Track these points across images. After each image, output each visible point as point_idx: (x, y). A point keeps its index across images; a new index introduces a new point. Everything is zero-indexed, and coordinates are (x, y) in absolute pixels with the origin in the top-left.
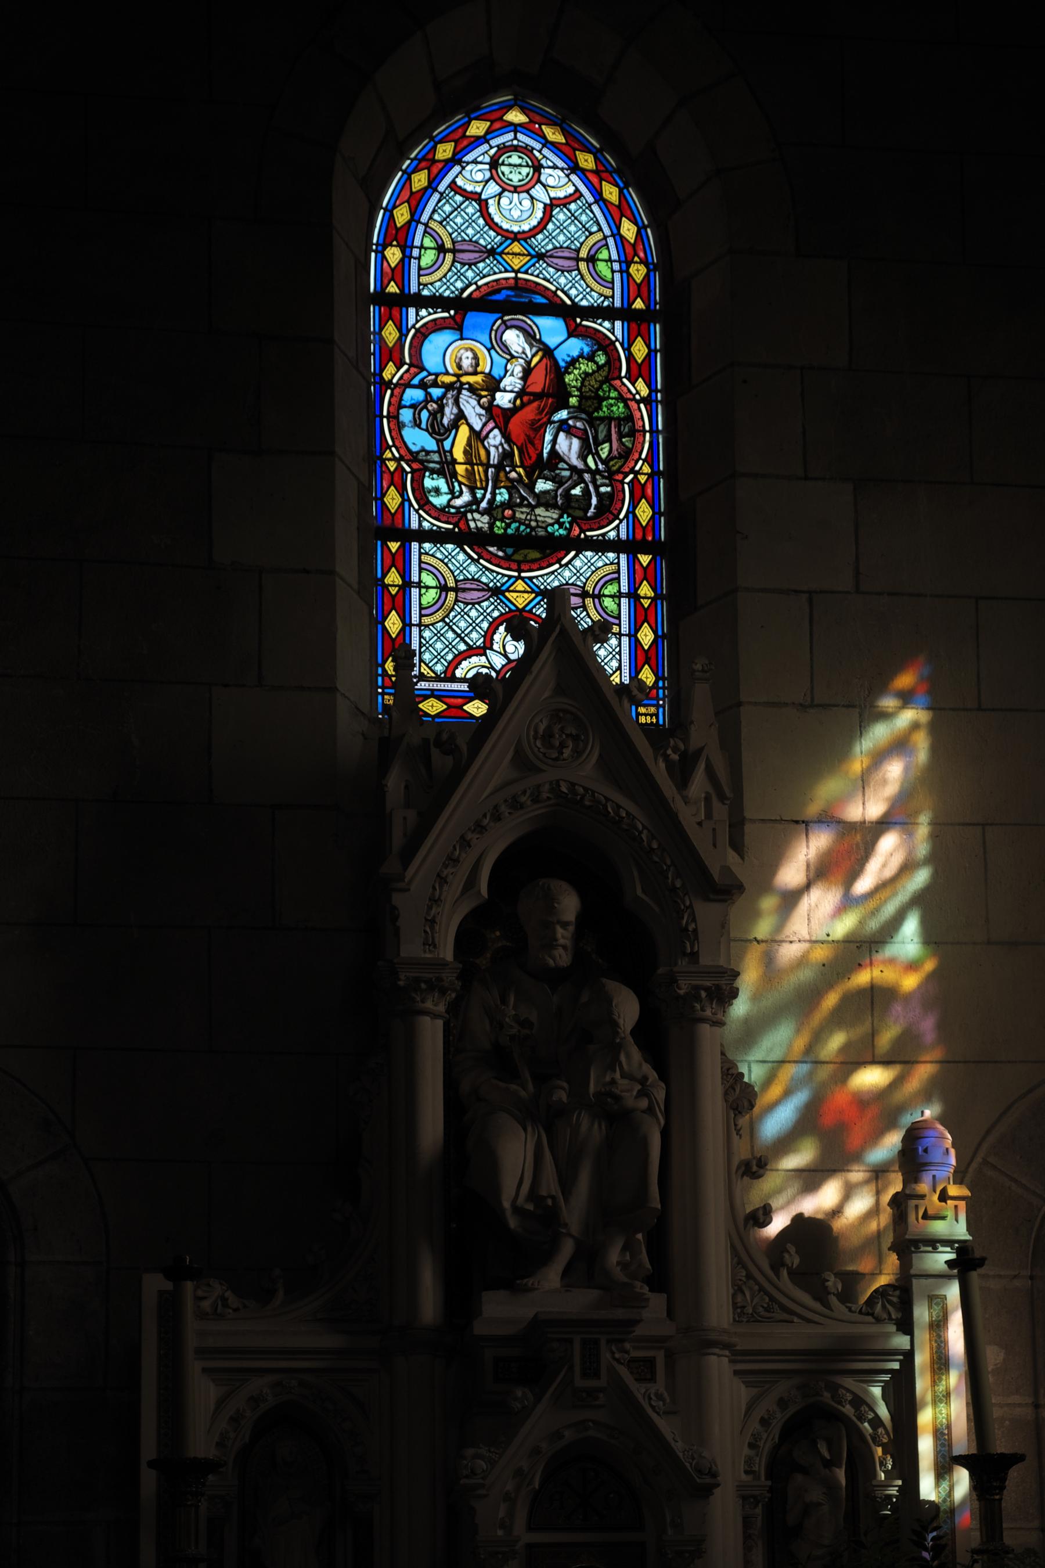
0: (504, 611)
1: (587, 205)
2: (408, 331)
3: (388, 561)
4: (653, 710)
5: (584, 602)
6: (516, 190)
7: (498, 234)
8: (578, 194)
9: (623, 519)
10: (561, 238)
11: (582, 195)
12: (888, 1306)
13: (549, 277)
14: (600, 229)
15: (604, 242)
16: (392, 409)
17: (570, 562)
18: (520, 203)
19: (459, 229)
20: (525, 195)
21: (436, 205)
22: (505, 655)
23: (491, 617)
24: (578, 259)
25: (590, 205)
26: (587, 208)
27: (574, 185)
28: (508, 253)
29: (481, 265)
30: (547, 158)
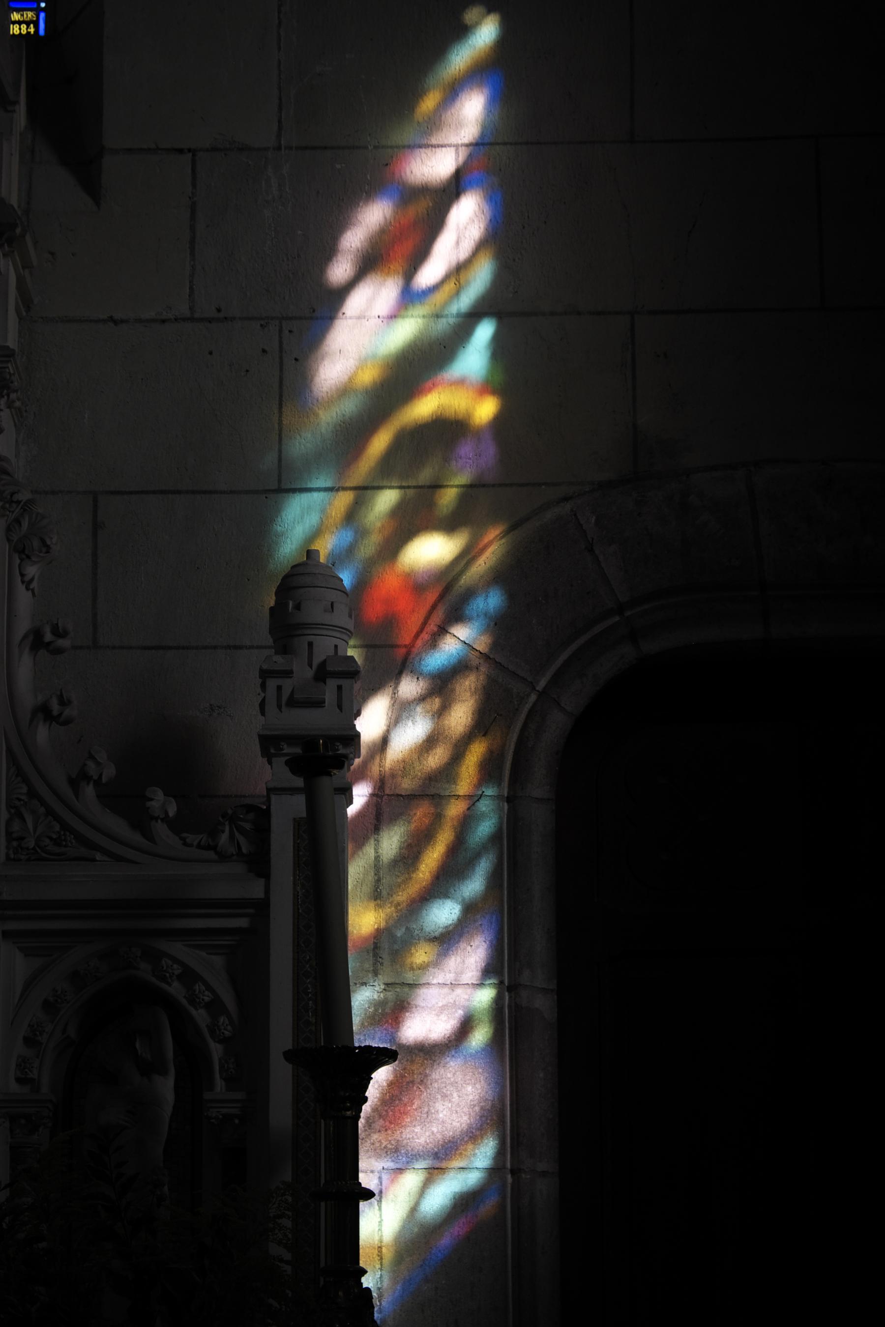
4: (30, 15)
12: (237, 834)
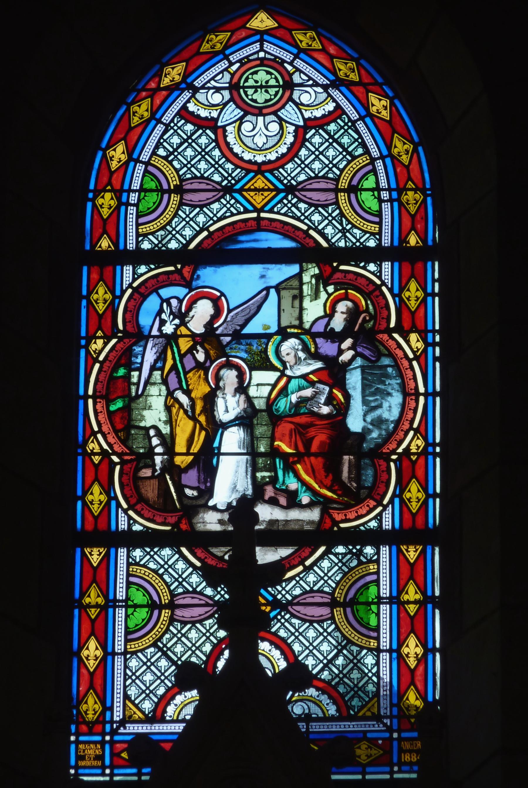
0: (281, 170)
1: (350, 124)
2: (123, 292)
3: (89, 576)
5: (332, 613)
6: (259, 112)
7: (237, 167)
8: (339, 112)
9: (127, 289)
10: (317, 165)
11: (344, 113)
13: (299, 214)
14: (367, 152)
15: (370, 167)
16: (413, 404)
17: (198, 233)
18: (267, 129)
19: (189, 164)
20: (273, 117)
21: (161, 137)
22: (281, 121)
23: (216, 638)
24: (336, 191)
25: (354, 122)
26: (349, 127)
27: (334, 101)
28: (249, 190)
29: (216, 206)
30: (301, 72)
